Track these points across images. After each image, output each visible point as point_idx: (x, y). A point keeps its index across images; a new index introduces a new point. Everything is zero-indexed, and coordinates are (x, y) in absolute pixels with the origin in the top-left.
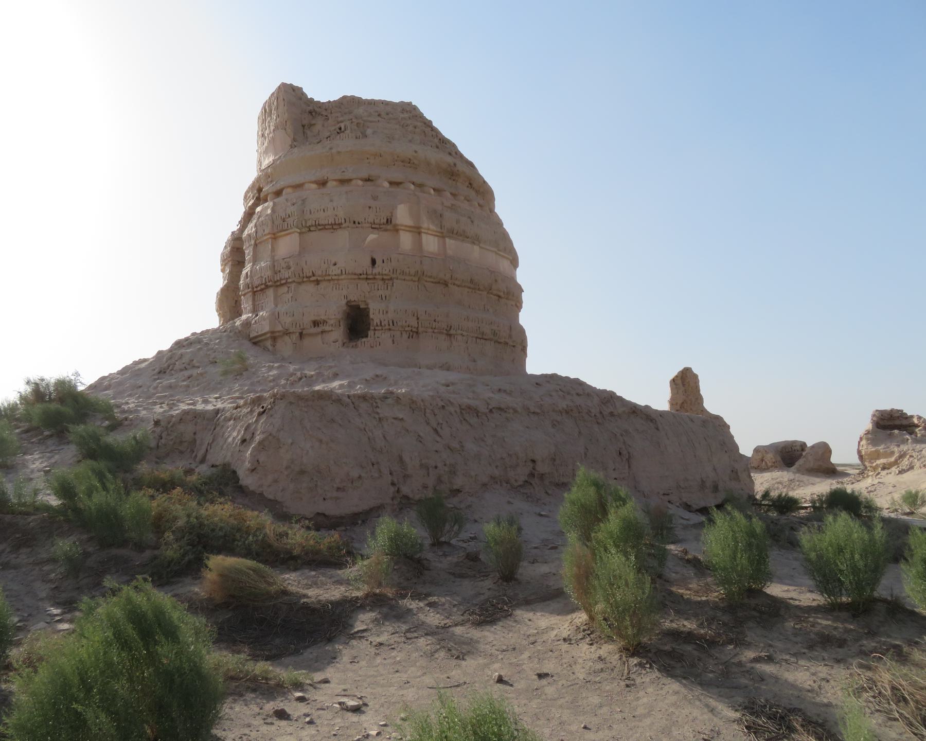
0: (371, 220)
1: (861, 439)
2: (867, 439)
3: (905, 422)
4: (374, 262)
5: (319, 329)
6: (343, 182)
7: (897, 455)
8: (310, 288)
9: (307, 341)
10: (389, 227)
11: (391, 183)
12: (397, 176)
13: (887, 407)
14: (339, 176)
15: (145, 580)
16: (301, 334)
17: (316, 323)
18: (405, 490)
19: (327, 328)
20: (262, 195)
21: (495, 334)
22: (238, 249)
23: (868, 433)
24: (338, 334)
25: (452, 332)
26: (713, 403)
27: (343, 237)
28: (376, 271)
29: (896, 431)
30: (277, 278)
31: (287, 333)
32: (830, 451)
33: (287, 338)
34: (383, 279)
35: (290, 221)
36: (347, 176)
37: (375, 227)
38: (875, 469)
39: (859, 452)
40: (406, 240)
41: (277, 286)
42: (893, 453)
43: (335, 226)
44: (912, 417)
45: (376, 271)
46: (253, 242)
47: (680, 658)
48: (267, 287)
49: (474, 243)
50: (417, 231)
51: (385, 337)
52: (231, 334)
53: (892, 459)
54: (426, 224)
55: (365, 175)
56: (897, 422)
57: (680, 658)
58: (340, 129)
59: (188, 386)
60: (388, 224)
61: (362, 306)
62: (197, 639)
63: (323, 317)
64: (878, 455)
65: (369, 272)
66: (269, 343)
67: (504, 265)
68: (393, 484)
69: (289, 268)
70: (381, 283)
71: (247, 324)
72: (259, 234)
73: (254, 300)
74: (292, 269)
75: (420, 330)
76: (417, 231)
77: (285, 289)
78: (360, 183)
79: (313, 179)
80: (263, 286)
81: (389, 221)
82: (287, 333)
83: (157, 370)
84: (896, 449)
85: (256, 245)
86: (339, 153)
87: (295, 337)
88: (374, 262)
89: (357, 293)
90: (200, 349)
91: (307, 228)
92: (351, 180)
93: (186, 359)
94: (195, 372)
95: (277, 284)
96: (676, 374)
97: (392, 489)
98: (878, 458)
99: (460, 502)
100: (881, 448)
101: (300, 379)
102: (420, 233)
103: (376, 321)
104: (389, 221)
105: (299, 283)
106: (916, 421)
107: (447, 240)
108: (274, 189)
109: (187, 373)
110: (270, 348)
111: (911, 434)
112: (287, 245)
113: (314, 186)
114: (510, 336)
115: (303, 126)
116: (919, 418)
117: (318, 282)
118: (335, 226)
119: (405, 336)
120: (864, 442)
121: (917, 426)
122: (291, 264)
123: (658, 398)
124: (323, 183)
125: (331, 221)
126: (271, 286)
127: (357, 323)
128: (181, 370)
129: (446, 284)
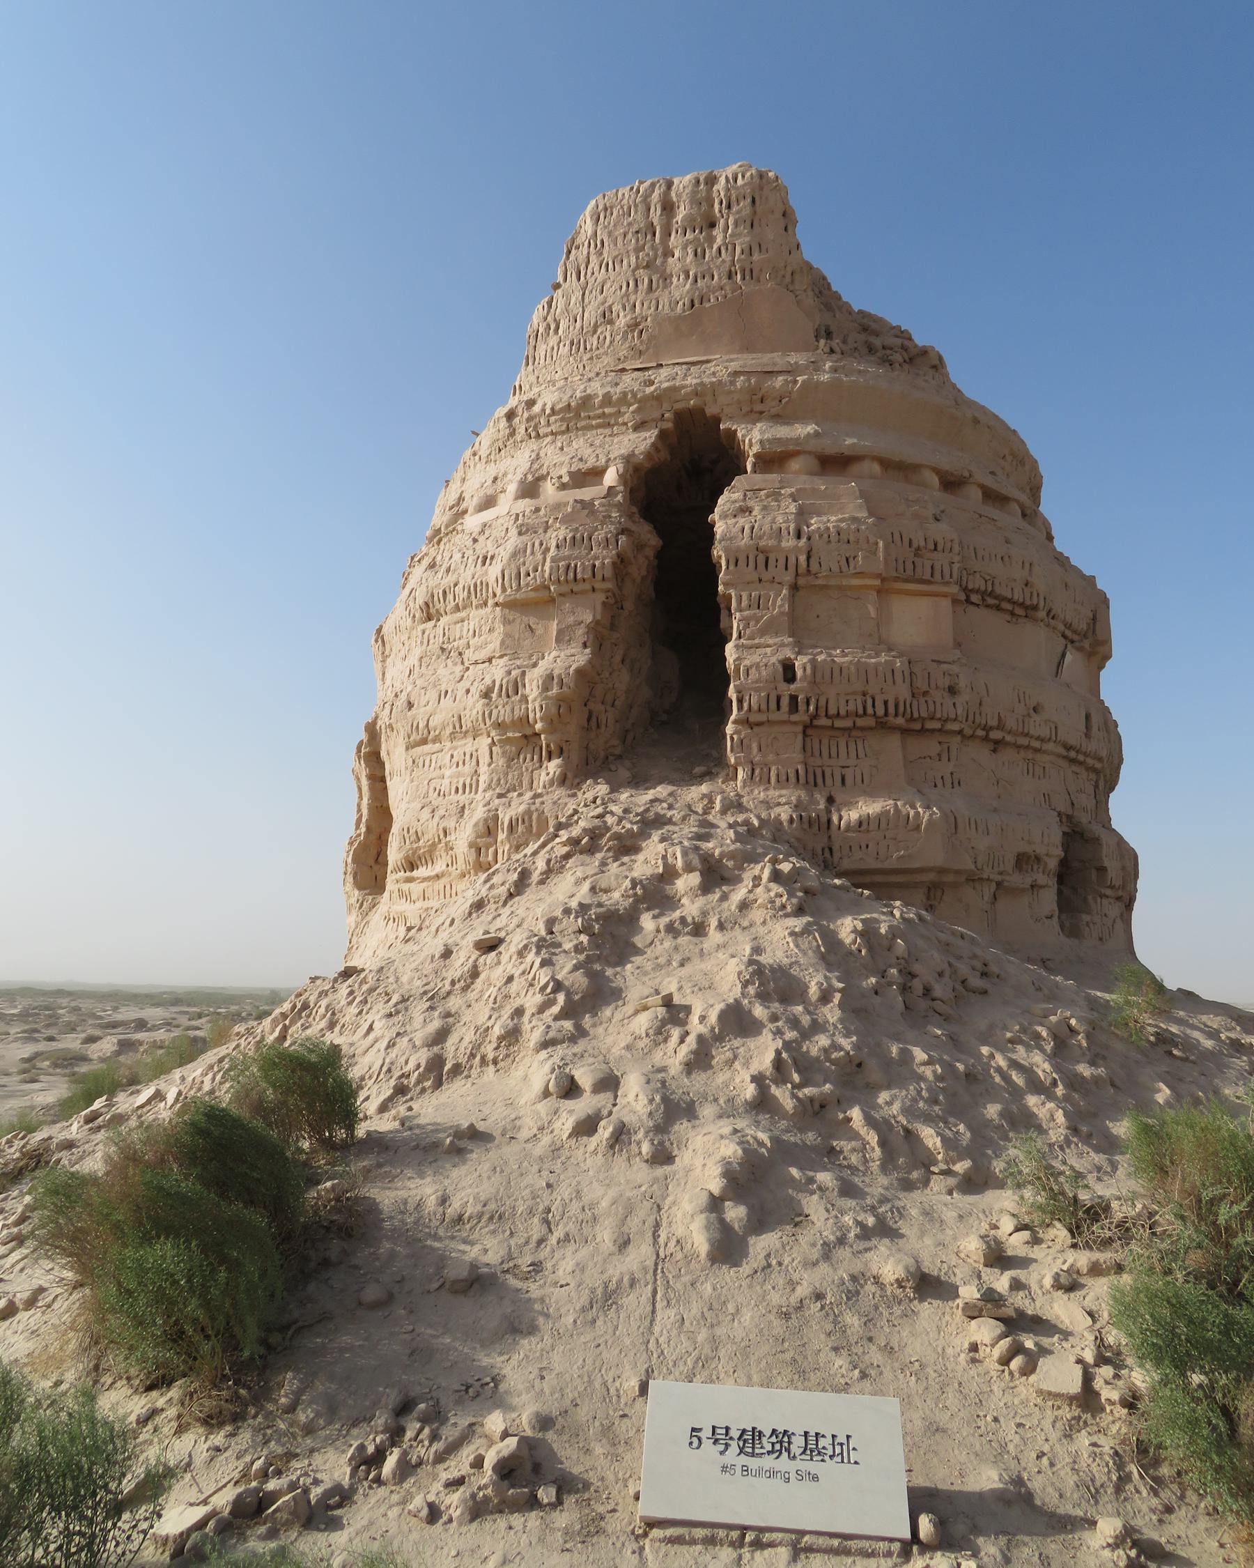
8: (980, 753)
14: (989, 482)
31: (973, 879)
35: (941, 560)
48: (882, 725)
69: (952, 691)
79: (945, 466)
82: (973, 879)
95: (914, 729)
113: (935, 481)
117: (997, 745)
122: (962, 683)
124: (951, 483)
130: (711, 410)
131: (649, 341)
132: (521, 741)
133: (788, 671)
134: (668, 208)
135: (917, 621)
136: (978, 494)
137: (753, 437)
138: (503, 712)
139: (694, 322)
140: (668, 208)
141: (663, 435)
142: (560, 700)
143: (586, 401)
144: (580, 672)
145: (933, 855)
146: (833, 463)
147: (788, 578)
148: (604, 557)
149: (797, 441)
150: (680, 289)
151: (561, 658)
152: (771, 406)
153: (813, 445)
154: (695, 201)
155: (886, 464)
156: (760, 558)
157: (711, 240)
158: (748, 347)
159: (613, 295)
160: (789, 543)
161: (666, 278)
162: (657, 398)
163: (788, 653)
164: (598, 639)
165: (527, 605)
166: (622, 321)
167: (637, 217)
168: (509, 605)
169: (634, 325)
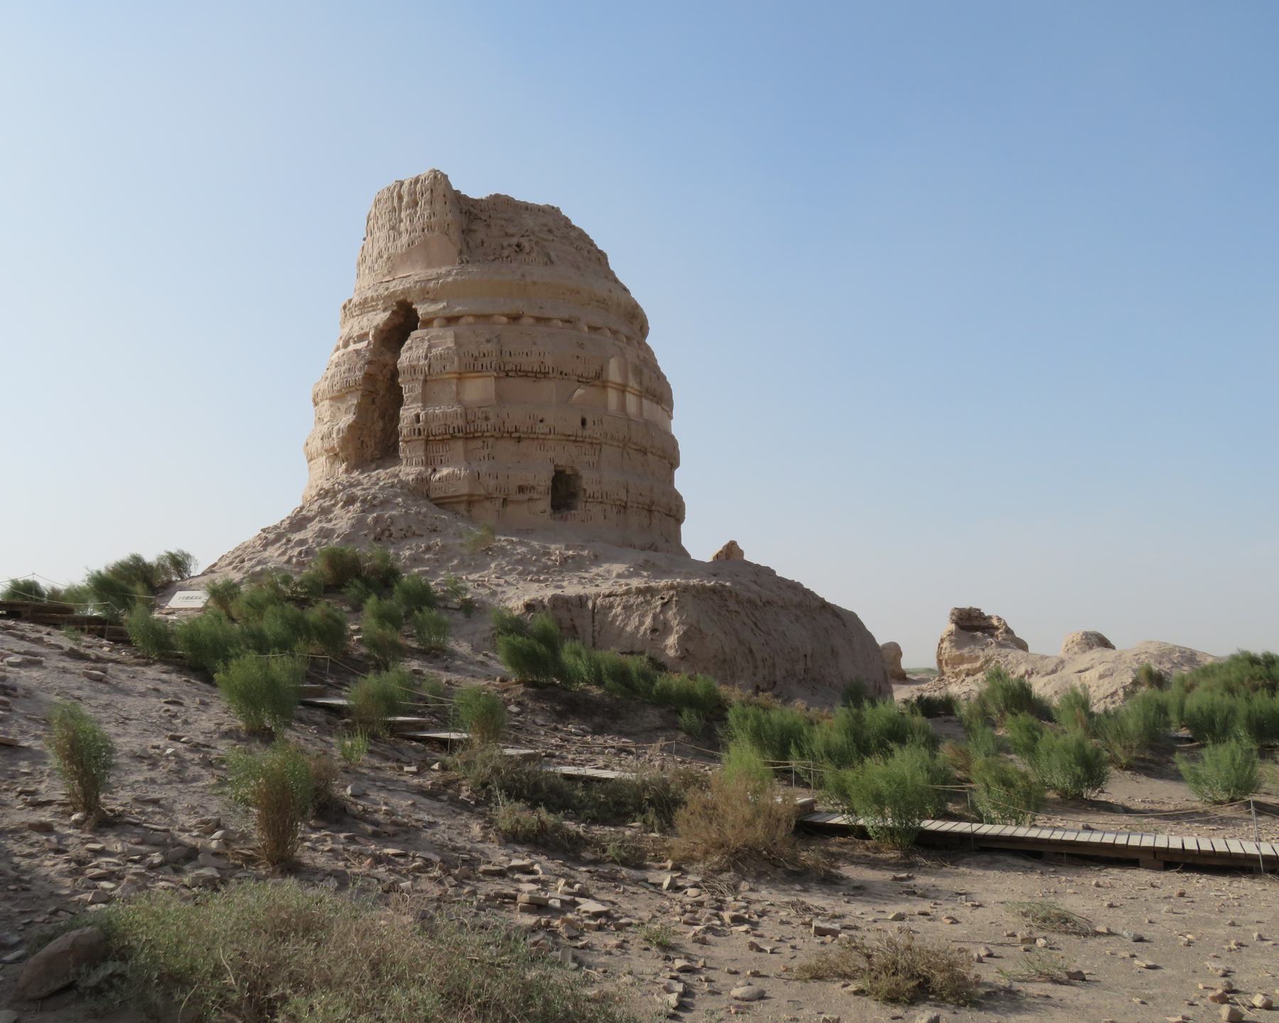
0: (579, 372)
1: (942, 641)
2: (951, 641)
3: (983, 623)
4: (584, 422)
5: (526, 497)
6: (539, 320)
7: (982, 660)
8: (510, 445)
9: (510, 509)
10: (597, 383)
11: (589, 327)
12: (597, 320)
13: (966, 604)
14: (536, 313)
16: (505, 500)
17: (521, 489)
19: (535, 496)
23: (951, 634)
24: (545, 503)
27: (548, 388)
28: (587, 433)
29: (979, 634)
31: (488, 498)
32: (901, 654)
33: (487, 504)
34: (591, 443)
35: (486, 361)
36: (547, 313)
37: (582, 381)
39: (939, 654)
40: (613, 396)
41: (467, 438)
42: (977, 658)
43: (541, 375)
44: (990, 617)
45: (587, 433)
47: (1151, 769)
48: (453, 437)
50: (623, 389)
51: (596, 510)
53: (978, 664)
54: (633, 383)
55: (566, 316)
56: (976, 623)
57: (1151, 769)
60: (598, 380)
61: (568, 472)
62: (154, 914)
63: (532, 483)
64: (961, 660)
65: (580, 433)
66: (462, 508)
69: (487, 419)
70: (588, 447)
74: (492, 421)
75: (629, 504)
76: (623, 389)
77: (479, 443)
78: (560, 324)
79: (506, 311)
81: (598, 376)
82: (488, 498)
84: (981, 653)
85: (425, 381)
86: (534, 283)
87: (499, 503)
88: (584, 422)
89: (566, 456)
91: (505, 373)
92: (549, 319)
95: (469, 437)
96: (720, 549)
98: (961, 663)
99: (118, 735)
100: (965, 651)
102: (623, 392)
103: (589, 491)
104: (598, 376)
105: (497, 439)
106: (995, 623)
107: (645, 402)
108: (448, 313)
110: (465, 513)
111: (992, 636)
112: (478, 390)
113: (504, 319)
116: (999, 619)
117: (519, 439)
118: (541, 375)
119: (615, 510)
120: (946, 644)
121: (997, 628)
122: (491, 416)
124: (515, 318)
125: (536, 368)
127: (564, 493)
129: (644, 452)
130: (409, 300)
131: (393, 263)
132: (334, 456)
133: (418, 416)
134: (400, 198)
135: (478, 390)
136: (531, 321)
137: (422, 310)
138: (327, 446)
139: (407, 256)
140: (400, 198)
141: (394, 312)
142: (343, 439)
143: (366, 299)
144: (350, 427)
145: (464, 489)
146: (451, 320)
147: (421, 378)
148: (359, 375)
149: (434, 313)
150: (405, 239)
151: (347, 419)
152: (431, 296)
153: (441, 314)
154: (410, 194)
155: (477, 316)
156: (413, 369)
157: (416, 212)
158: (430, 265)
159: (382, 244)
160: (422, 362)
161: (400, 234)
162: (389, 296)
163: (419, 410)
164: (361, 410)
165: (338, 398)
166: (385, 256)
167: (389, 203)
168: (332, 399)
169: (389, 258)
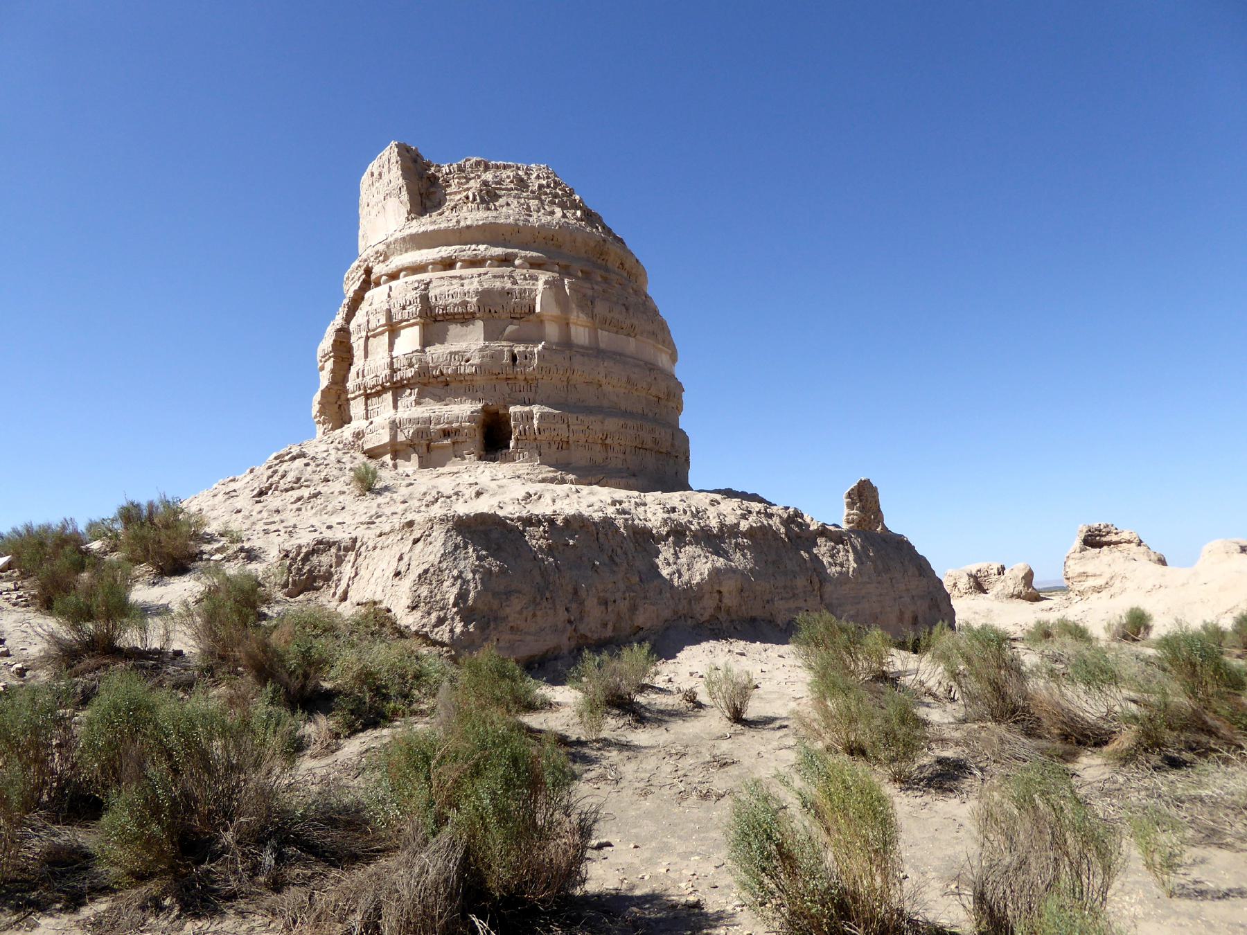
15: (657, 673)
18: (583, 628)
20: (373, 277)
21: (655, 442)
22: (341, 342)
25: (608, 441)
26: (895, 520)
30: (398, 377)
38: (1081, 593)
46: (364, 334)
49: (629, 335)
52: (340, 446)
58: (467, 198)
59: (299, 510)
67: (663, 360)
68: (570, 622)
71: (359, 435)
72: (372, 326)
73: (366, 404)
80: (379, 388)
83: (255, 492)
85: (367, 338)
90: (307, 465)
93: (291, 477)
94: (305, 492)
97: (570, 628)
101: (437, 500)
109: (295, 494)
114: (673, 445)
115: (421, 195)
122: (414, 361)
123: (839, 515)
126: (389, 388)
128: (287, 490)
